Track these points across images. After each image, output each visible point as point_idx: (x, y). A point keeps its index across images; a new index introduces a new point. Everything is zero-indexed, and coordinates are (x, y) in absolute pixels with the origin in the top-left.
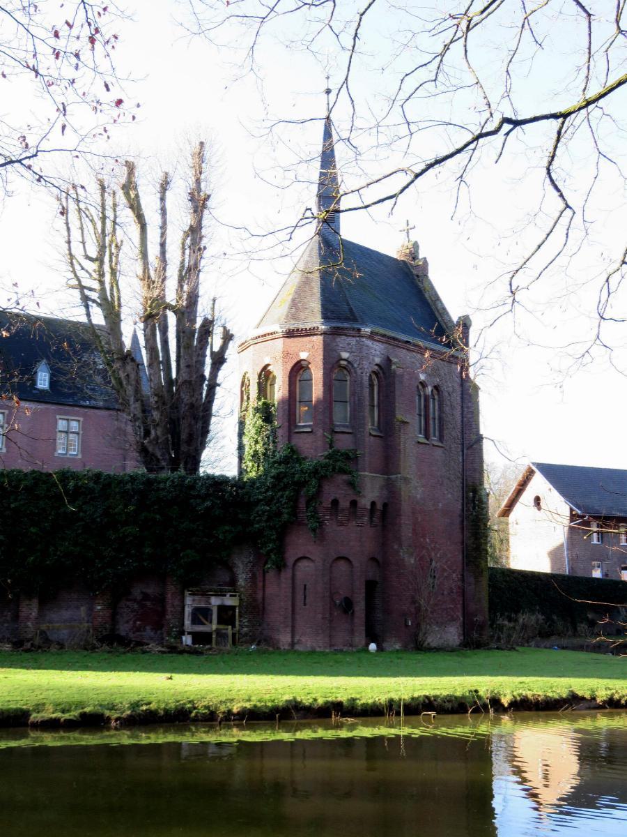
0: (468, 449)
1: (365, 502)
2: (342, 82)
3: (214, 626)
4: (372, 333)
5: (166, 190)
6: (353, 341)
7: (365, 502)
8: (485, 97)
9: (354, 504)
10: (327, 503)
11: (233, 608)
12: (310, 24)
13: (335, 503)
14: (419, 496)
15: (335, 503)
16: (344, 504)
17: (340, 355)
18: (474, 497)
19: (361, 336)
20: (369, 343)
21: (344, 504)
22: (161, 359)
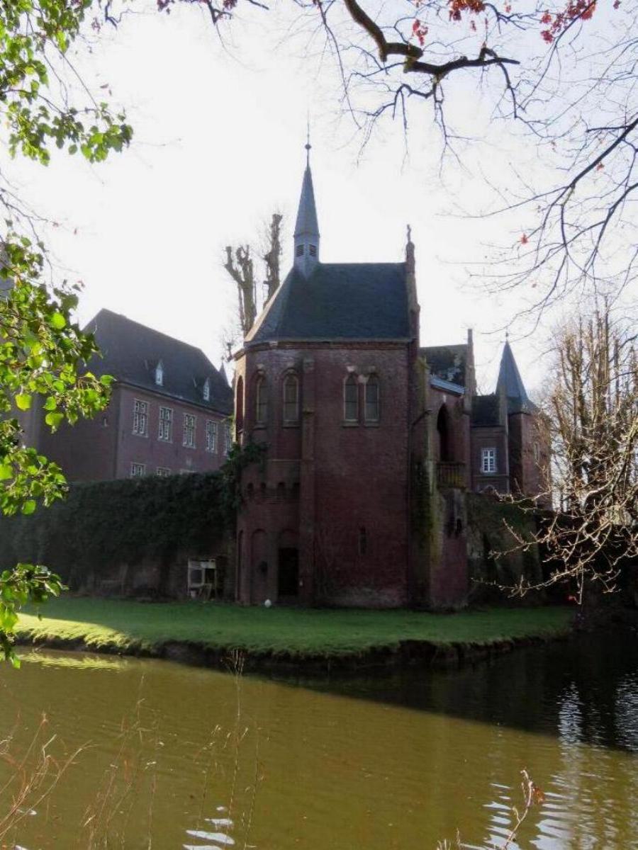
0: (256, 423)
1: (272, 484)
2: (601, 221)
3: (203, 584)
4: (279, 343)
5: (598, 324)
6: (266, 353)
7: (272, 484)
8: (406, 133)
9: (263, 485)
10: (244, 488)
11: (212, 570)
12: (534, 194)
13: (251, 486)
14: (343, 474)
15: (251, 486)
16: (257, 486)
17: (257, 367)
18: (419, 469)
19: (271, 349)
20: (280, 352)
21: (257, 486)
22: (207, 398)
